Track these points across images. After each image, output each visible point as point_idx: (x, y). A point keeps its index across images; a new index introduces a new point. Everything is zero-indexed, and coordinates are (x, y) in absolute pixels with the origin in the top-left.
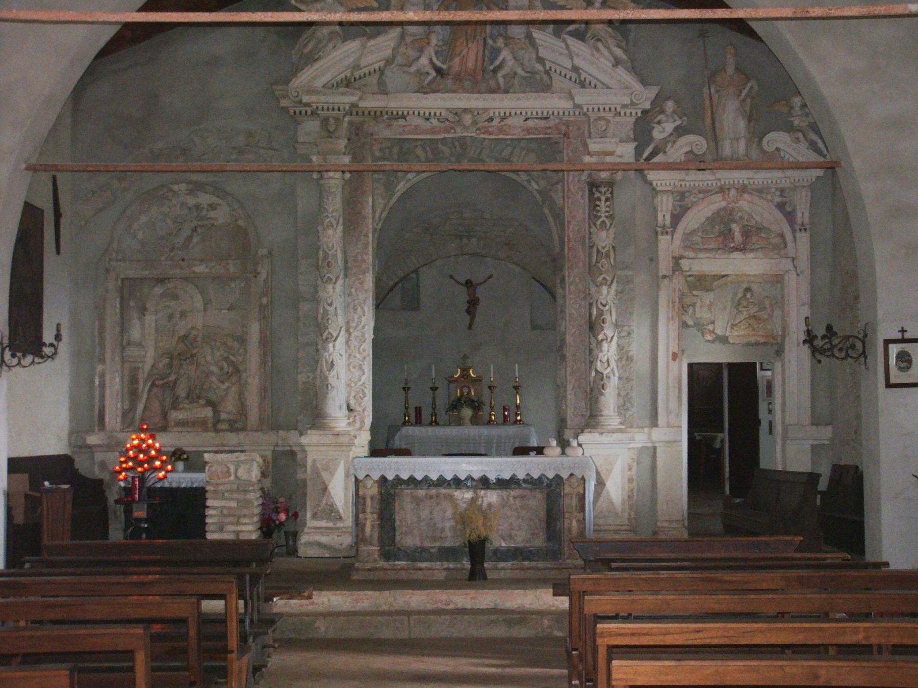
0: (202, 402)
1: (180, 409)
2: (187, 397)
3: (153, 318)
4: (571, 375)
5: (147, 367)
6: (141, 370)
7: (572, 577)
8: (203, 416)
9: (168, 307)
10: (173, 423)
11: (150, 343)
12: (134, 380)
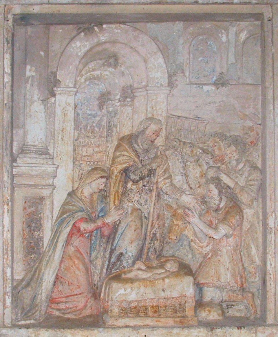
0: (171, 266)
1: (131, 281)
2: (139, 257)
3: (71, 100)
4: (5, 150)
5: (60, 198)
6: (48, 202)
7: (177, 227)
8: (175, 294)
9: (99, 78)
10: (116, 310)
11: (63, 149)
12: (33, 223)
